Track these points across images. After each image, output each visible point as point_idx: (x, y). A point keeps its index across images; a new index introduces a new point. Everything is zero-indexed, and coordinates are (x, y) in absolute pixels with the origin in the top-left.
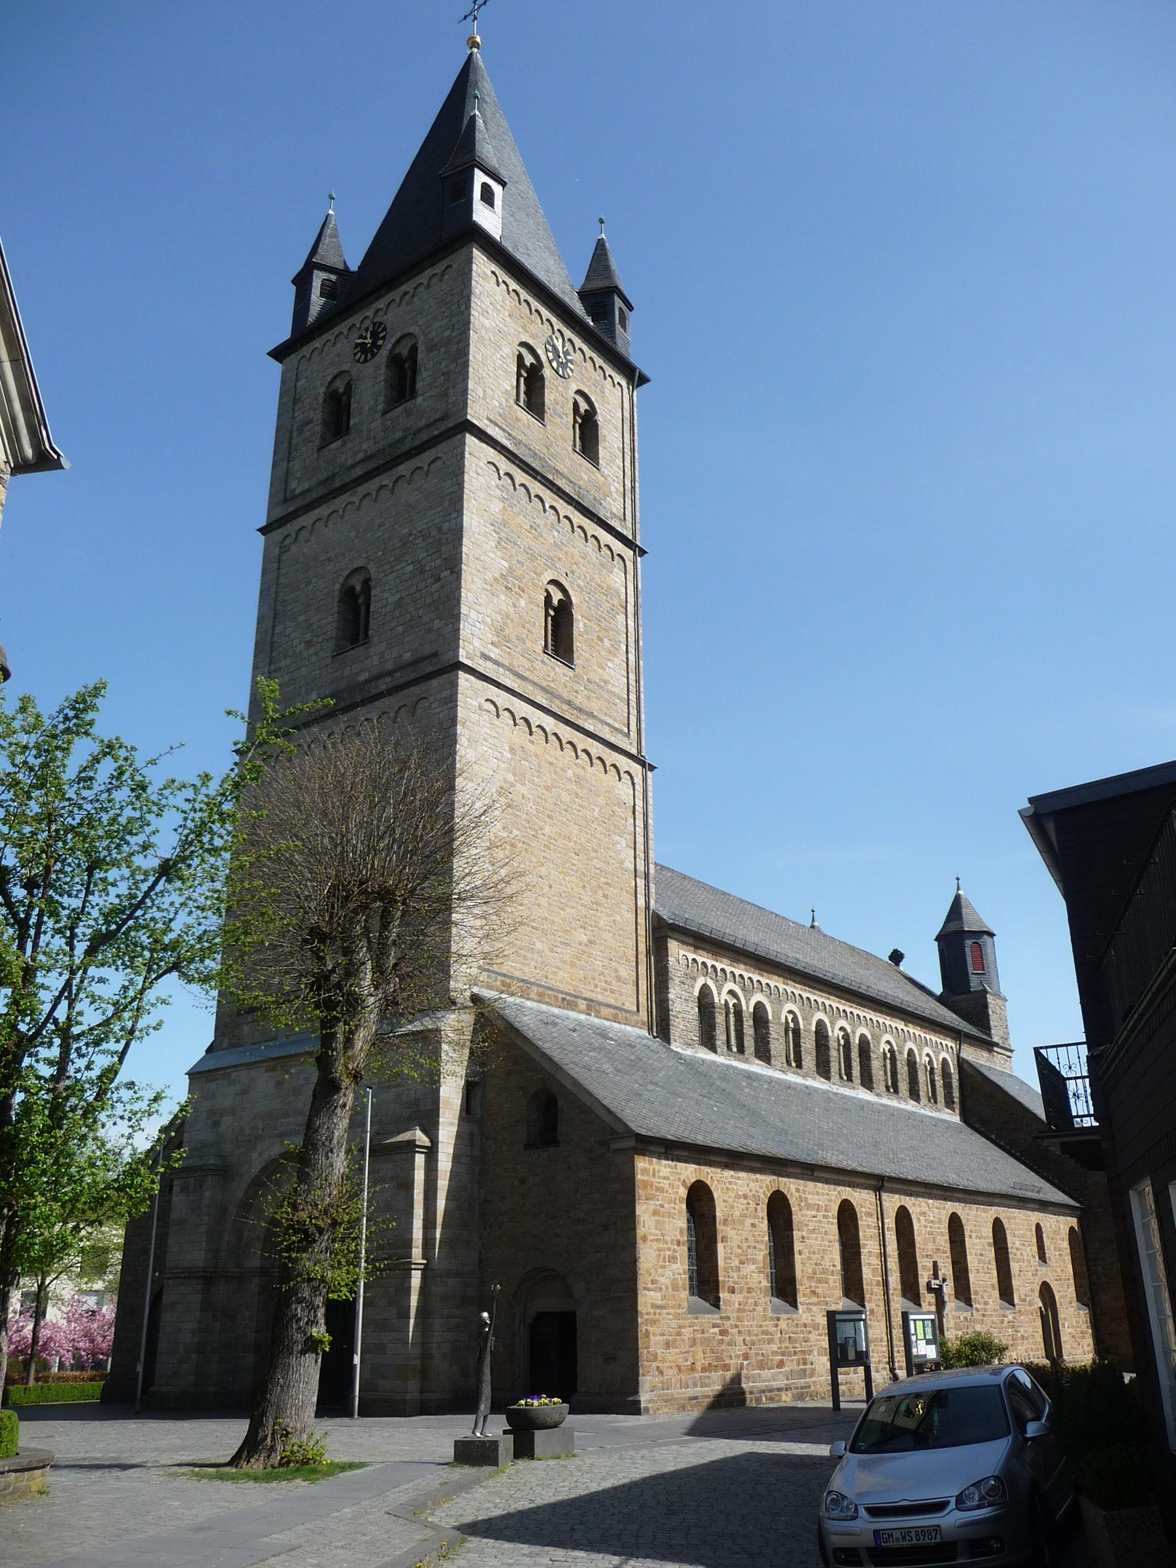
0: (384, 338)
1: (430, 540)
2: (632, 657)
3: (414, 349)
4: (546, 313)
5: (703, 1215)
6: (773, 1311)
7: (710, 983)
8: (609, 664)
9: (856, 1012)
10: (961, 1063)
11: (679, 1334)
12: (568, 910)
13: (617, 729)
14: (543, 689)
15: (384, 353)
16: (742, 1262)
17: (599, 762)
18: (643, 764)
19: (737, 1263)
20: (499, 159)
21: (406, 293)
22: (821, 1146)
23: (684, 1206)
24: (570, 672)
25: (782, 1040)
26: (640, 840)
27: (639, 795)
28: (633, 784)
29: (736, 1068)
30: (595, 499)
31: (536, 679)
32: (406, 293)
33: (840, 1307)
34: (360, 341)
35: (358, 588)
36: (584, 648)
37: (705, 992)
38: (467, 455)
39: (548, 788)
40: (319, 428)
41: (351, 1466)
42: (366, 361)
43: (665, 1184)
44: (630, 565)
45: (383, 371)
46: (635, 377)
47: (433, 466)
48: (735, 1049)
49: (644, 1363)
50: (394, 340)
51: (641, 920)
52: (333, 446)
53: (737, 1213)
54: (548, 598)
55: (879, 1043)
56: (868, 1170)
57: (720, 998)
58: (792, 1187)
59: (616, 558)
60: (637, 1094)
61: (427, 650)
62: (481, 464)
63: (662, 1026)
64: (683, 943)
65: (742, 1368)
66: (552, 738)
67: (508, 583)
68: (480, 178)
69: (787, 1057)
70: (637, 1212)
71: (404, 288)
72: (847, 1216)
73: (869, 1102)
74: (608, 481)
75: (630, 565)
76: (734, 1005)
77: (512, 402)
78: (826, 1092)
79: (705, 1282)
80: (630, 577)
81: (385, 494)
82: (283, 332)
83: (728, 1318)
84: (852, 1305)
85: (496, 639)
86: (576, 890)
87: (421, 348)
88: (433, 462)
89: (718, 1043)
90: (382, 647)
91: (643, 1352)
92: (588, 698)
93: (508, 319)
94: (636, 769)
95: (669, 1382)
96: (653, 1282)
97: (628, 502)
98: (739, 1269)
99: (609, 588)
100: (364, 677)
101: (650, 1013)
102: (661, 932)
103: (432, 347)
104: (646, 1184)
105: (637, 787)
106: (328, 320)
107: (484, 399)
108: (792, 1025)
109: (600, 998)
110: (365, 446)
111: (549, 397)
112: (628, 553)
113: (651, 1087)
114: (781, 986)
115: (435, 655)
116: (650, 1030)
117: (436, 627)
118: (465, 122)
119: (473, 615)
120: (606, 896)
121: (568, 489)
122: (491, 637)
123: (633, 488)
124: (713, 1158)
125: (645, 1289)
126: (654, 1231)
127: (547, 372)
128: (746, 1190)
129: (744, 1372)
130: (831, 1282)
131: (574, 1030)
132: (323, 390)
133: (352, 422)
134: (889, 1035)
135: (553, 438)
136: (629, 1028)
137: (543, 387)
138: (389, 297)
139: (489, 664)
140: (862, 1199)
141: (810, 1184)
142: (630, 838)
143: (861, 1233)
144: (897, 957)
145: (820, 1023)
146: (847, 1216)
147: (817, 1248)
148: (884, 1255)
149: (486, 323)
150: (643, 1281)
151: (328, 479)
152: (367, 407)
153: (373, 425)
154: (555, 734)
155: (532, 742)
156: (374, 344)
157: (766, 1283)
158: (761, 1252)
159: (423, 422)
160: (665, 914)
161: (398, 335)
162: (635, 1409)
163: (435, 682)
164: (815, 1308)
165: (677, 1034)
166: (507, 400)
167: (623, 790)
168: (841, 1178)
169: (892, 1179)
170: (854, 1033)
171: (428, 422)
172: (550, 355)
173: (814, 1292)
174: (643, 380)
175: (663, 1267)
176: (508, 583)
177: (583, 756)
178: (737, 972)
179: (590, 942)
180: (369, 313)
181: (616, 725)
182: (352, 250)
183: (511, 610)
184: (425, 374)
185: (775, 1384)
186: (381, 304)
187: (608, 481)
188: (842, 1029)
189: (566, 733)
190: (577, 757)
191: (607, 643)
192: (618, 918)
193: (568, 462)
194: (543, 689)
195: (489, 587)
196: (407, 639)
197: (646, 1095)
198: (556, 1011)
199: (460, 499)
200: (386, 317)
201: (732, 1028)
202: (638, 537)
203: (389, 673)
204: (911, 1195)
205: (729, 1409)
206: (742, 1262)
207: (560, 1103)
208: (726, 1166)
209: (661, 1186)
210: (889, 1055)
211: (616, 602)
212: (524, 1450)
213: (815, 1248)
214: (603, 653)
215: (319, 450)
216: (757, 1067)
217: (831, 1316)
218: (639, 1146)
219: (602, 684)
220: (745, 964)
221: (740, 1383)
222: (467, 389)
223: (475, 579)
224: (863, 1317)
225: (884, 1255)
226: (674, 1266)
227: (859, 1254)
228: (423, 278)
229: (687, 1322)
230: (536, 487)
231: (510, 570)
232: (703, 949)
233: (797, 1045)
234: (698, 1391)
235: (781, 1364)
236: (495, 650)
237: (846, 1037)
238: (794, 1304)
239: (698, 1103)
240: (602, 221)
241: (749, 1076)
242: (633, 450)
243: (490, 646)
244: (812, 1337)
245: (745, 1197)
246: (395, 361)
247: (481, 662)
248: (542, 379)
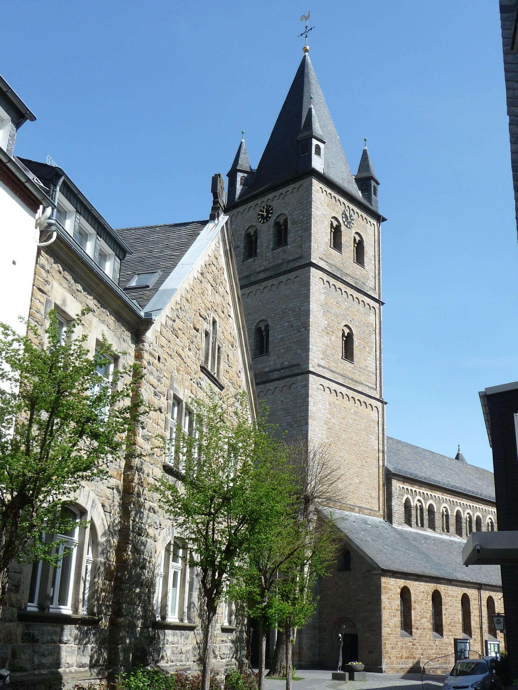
0: (272, 213)
1: (295, 313)
2: (378, 353)
3: (286, 221)
4: (342, 200)
5: (406, 599)
7: (410, 497)
8: (368, 358)
9: (475, 505)
11: (397, 644)
12: (351, 470)
13: (371, 388)
14: (341, 375)
15: (272, 221)
16: (421, 618)
17: (364, 404)
18: (382, 402)
19: (419, 618)
20: (323, 131)
21: (282, 194)
22: (455, 570)
23: (399, 596)
24: (352, 365)
25: (441, 520)
26: (381, 436)
27: (380, 416)
28: (378, 411)
29: (420, 534)
30: (363, 283)
33: (461, 637)
34: (261, 213)
35: (263, 329)
36: (358, 353)
37: (407, 501)
38: (311, 277)
39: (343, 419)
40: (242, 251)
41: (302, 679)
42: (263, 223)
43: (392, 587)
44: (377, 311)
45: (272, 229)
46: (379, 219)
47: (296, 279)
48: (420, 525)
49: (384, 654)
50: (277, 215)
51: (381, 471)
52: (249, 260)
53: (420, 599)
55: (485, 519)
56: (475, 581)
57: (414, 503)
58: (442, 588)
60: (381, 550)
61: (295, 362)
62: (317, 280)
63: (389, 517)
64: (398, 480)
65: (420, 658)
66: (345, 396)
67: (328, 331)
68: (315, 142)
69: (443, 527)
70: (382, 598)
71: (280, 191)
72: (465, 600)
74: (367, 275)
75: (377, 311)
76: (420, 506)
77: (328, 247)
79: (407, 625)
80: (377, 316)
81: (274, 288)
83: (416, 639)
84: (466, 636)
85: (323, 357)
86: (355, 461)
87: (289, 222)
88: (296, 277)
89: (413, 523)
90: (275, 357)
91: (383, 650)
92: (359, 375)
94: (379, 404)
95: (393, 662)
96: (387, 624)
97: (377, 280)
98: (420, 620)
100: (267, 369)
101: (384, 511)
102: (389, 476)
103: (294, 223)
104: (344, 251)
105: (379, 413)
106: (245, 199)
107: (318, 249)
108: (445, 513)
109: (364, 506)
110: (264, 263)
111: (344, 239)
112: (376, 305)
113: (386, 547)
114: (441, 496)
115: (298, 365)
116: (384, 518)
117: (299, 352)
119: (314, 348)
120: (366, 462)
122: (321, 356)
123: (379, 273)
124: (411, 577)
125: (385, 627)
126: (388, 605)
127: (343, 228)
128: (423, 589)
129: (421, 660)
130: (458, 627)
131: (355, 522)
132: (244, 232)
133: (258, 251)
136: (375, 518)
137: (341, 235)
138: (274, 194)
140: (472, 593)
141: (450, 587)
142: (376, 435)
143: (471, 607)
145: (458, 512)
146: (465, 600)
147: (452, 612)
148: (481, 616)
149: (318, 213)
150: (384, 624)
151: (248, 276)
152: (265, 245)
153: (268, 254)
154: (347, 395)
155: (337, 400)
156: (267, 215)
157: (431, 626)
158: (429, 614)
160: (391, 468)
161: (279, 213)
162: (380, 671)
163: (299, 377)
164: (450, 637)
165: (395, 520)
166: (326, 247)
167: (374, 414)
168: (463, 584)
169: (485, 585)
170: (474, 515)
171: (294, 258)
172: (344, 219)
173: (450, 631)
174: (384, 220)
175: (391, 619)
176: (328, 331)
178: (421, 491)
179: (360, 482)
180: (265, 200)
181: (371, 386)
182: (252, 160)
183: (329, 342)
184: (291, 235)
185: (435, 666)
186: (270, 196)
187: (367, 275)
188: (468, 513)
189: (351, 393)
190: (355, 403)
191: (367, 349)
192: (371, 471)
193: (351, 269)
195: (320, 334)
196: (286, 356)
197: (385, 551)
199: (308, 297)
201: (419, 516)
203: (279, 370)
204: (494, 591)
205: (416, 671)
206: (421, 618)
207: (352, 554)
208: (416, 580)
209: (391, 588)
210: (490, 524)
211: (371, 329)
212: (352, 678)
213: (451, 613)
214: (366, 354)
215: (243, 261)
216: (429, 533)
217: (455, 640)
218: (383, 573)
219: (365, 368)
220: (425, 487)
221: (419, 664)
222: (311, 246)
223: (315, 332)
224: (468, 641)
225: (481, 616)
226: (395, 619)
227: (470, 616)
228: (290, 188)
229: (400, 640)
230: (339, 284)
232: (407, 482)
233: (447, 522)
234: (404, 666)
236: (323, 361)
237: (470, 517)
238: (442, 635)
239: (405, 553)
240: (365, 140)
241: (426, 538)
242: (379, 255)
244: (449, 648)
245: (423, 592)
246: (277, 224)
247: (318, 368)
248: (341, 231)
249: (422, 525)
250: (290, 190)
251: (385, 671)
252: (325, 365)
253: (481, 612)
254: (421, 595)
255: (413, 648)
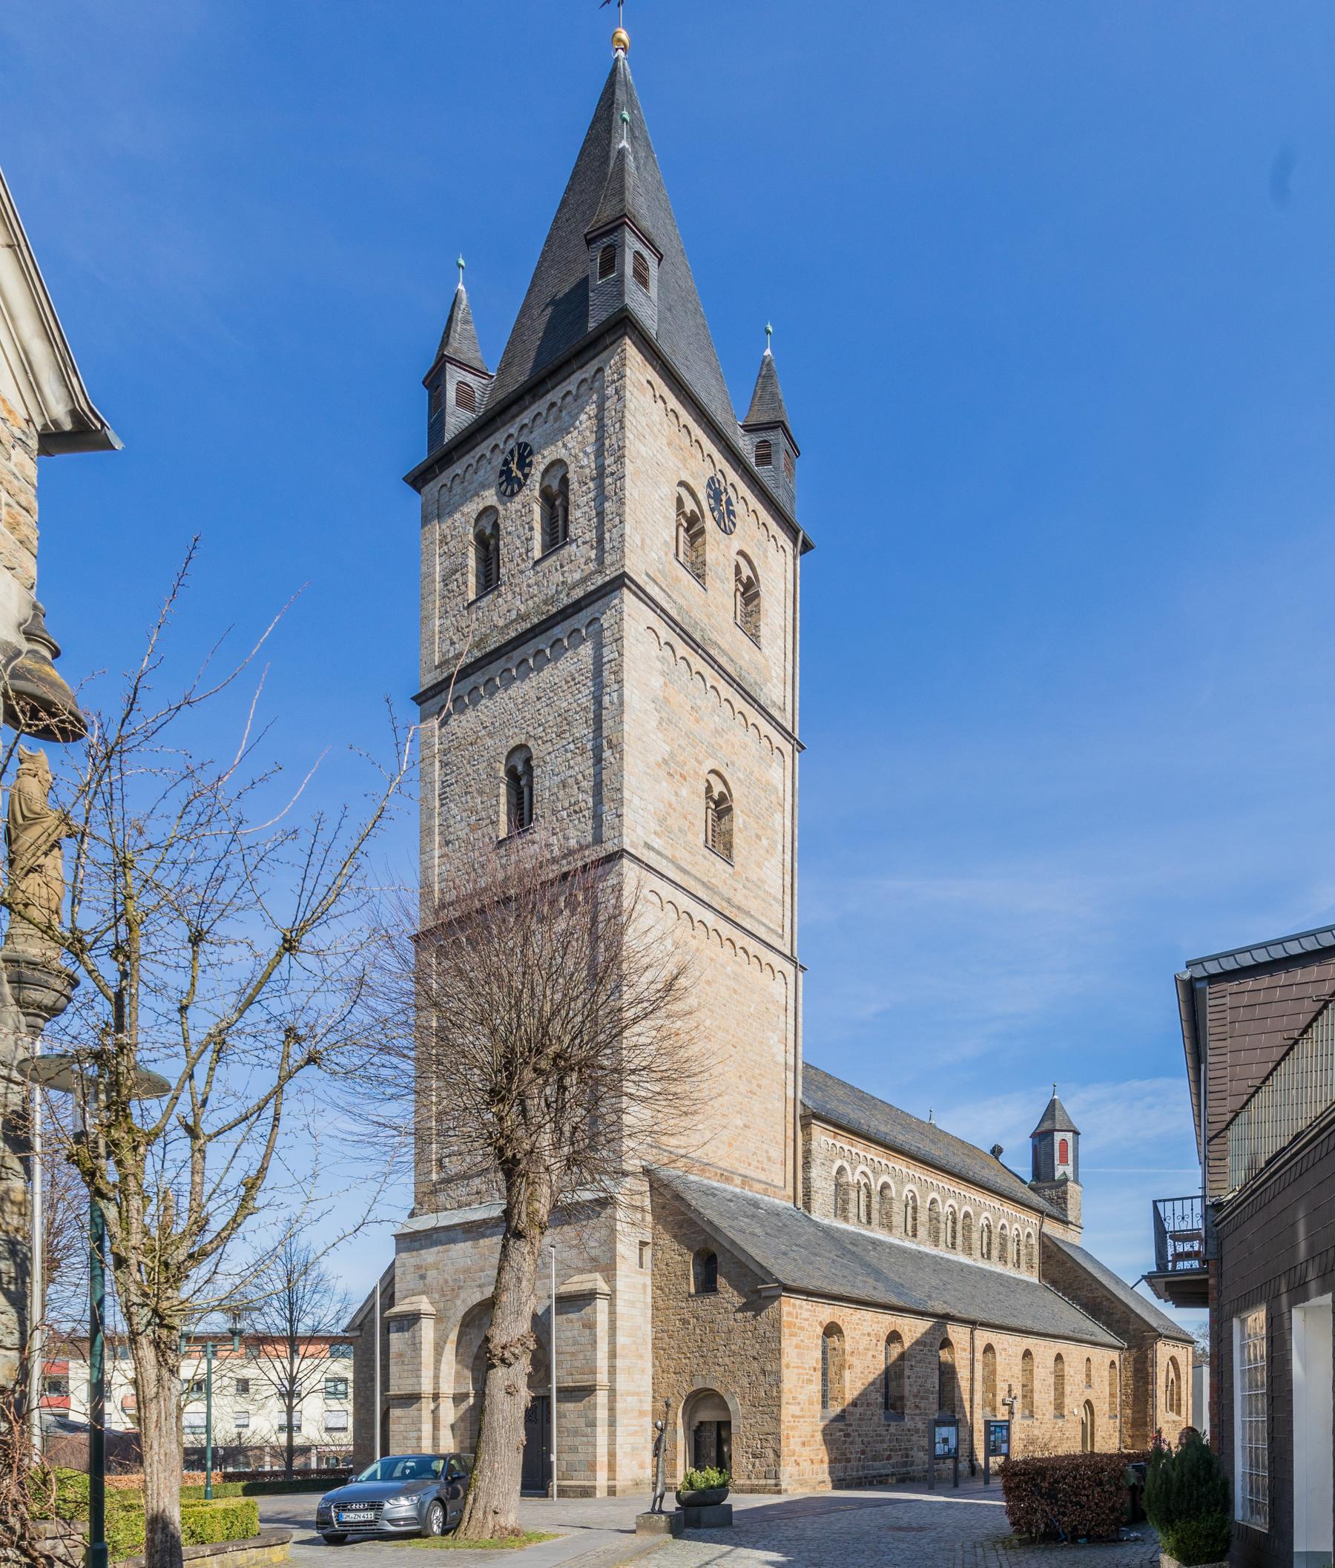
6: (886, 1418)
7: (846, 1165)
10: (1042, 1235)
14: (703, 884)
22: (930, 1297)
31: (698, 875)
32: (553, 405)
35: (520, 768)
43: (805, 1324)
53: (861, 1348)
54: (709, 789)
57: (852, 1177)
59: (776, 751)
67: (671, 768)
71: (550, 397)
73: (968, 1266)
77: (672, 556)
78: (934, 1257)
82: (419, 454)
85: (658, 829)
92: (746, 897)
93: (666, 449)
94: (789, 969)
96: (794, 1398)
99: (768, 783)
102: (808, 1118)
104: (791, 1325)
107: (642, 548)
109: (752, 1174)
111: (711, 555)
113: (794, 1248)
114: (905, 1170)
118: (613, 154)
119: (636, 800)
120: (759, 1086)
121: (730, 669)
122: (653, 826)
127: (710, 524)
128: (869, 1330)
134: (987, 1210)
135: (713, 607)
139: (652, 854)
144: (997, 1151)
149: (643, 450)
159: (577, 576)
173: (917, 1407)
176: (671, 768)
177: (740, 952)
181: (772, 926)
183: (673, 799)
185: (883, 1472)
186: (526, 418)
189: (726, 930)
191: (764, 841)
192: (770, 1106)
194: (703, 884)
198: (716, 1184)
200: (533, 435)
202: (797, 731)
203: (554, 860)
230: (698, 664)
231: (672, 754)
235: (889, 1458)
237: (953, 1213)
239: (833, 1261)
243: (653, 836)
244: (914, 1438)
245: (869, 1335)
247: (645, 851)
249: (869, 1222)
250: (573, 388)
251: (786, 1490)
252: (661, 849)
253: (972, 1372)
254: (864, 1342)
255: (845, 1442)
